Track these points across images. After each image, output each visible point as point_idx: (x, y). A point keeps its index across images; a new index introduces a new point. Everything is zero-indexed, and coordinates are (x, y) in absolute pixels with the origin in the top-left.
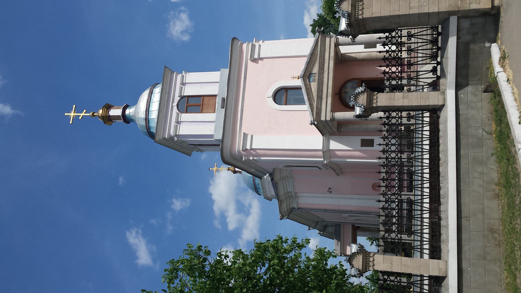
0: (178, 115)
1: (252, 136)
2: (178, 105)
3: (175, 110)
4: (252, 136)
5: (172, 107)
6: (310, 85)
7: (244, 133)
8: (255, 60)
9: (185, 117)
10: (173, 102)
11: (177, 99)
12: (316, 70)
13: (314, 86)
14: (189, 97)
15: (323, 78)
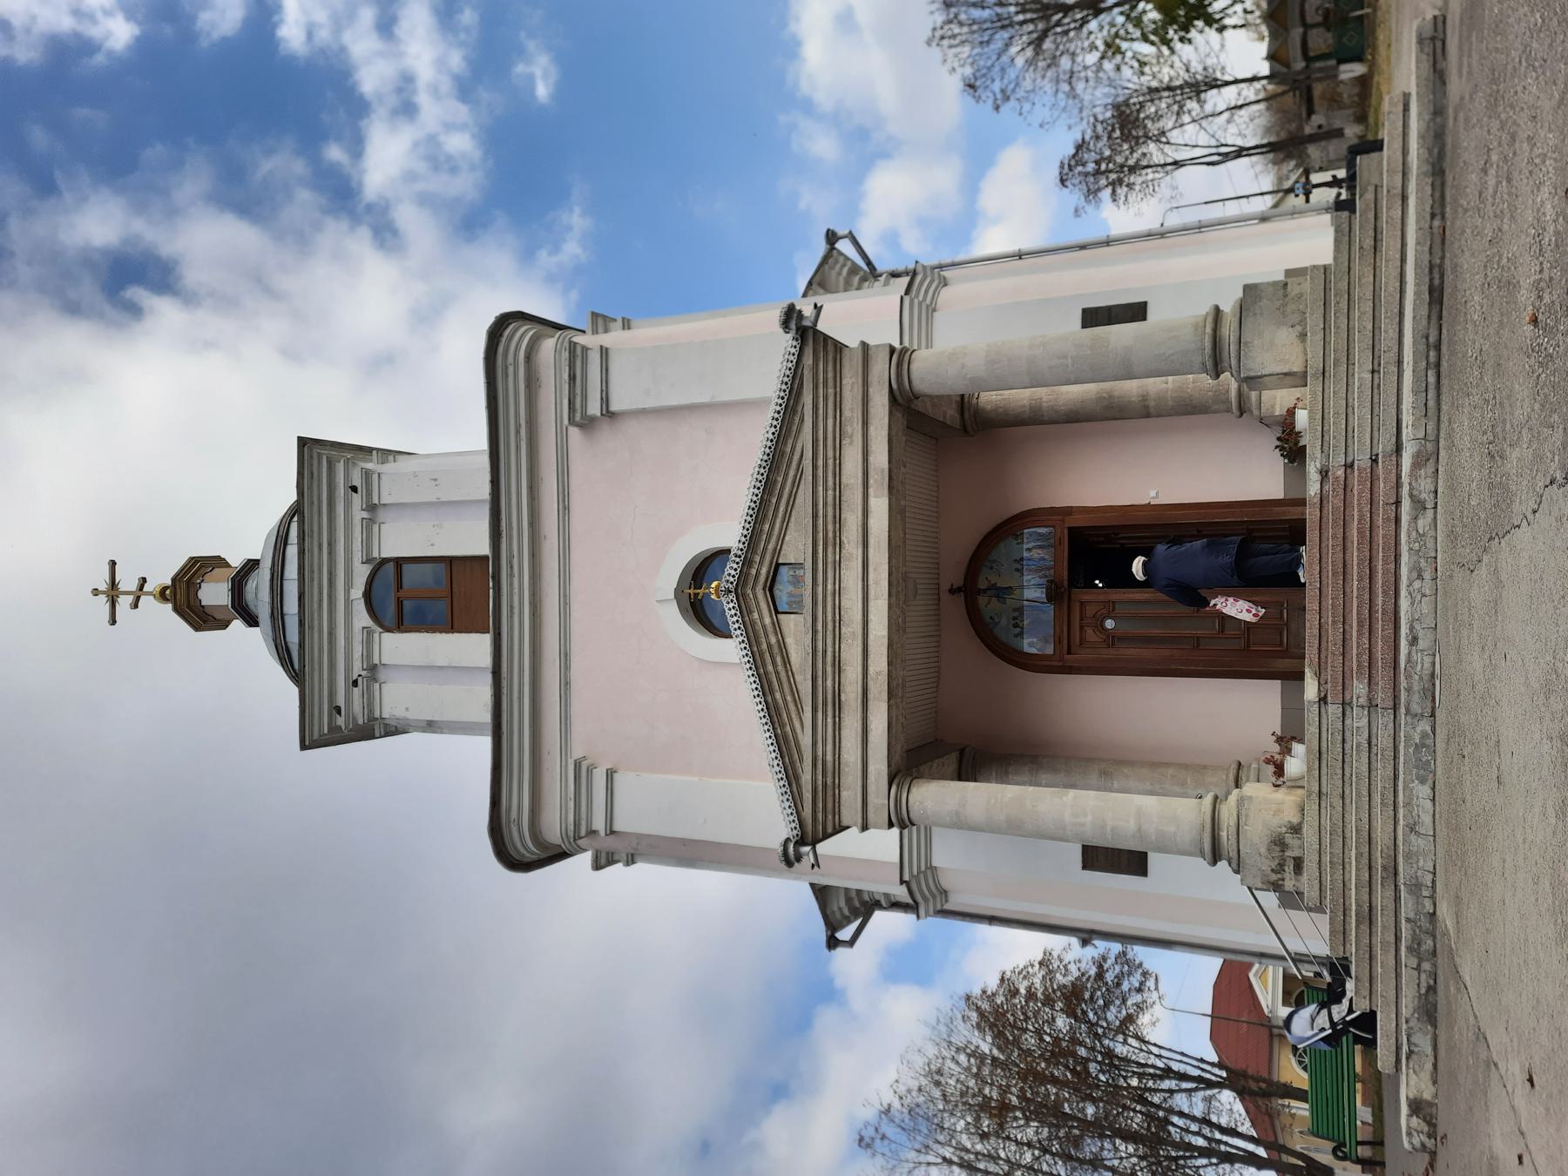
0: (368, 632)
1: (610, 774)
2: (368, 595)
3: (362, 618)
4: (610, 774)
5: (348, 603)
6: (777, 627)
7: (578, 765)
8: (589, 425)
9: (398, 647)
10: (349, 586)
11: (362, 573)
12: (796, 546)
13: (795, 629)
14: (399, 562)
15: (837, 593)
